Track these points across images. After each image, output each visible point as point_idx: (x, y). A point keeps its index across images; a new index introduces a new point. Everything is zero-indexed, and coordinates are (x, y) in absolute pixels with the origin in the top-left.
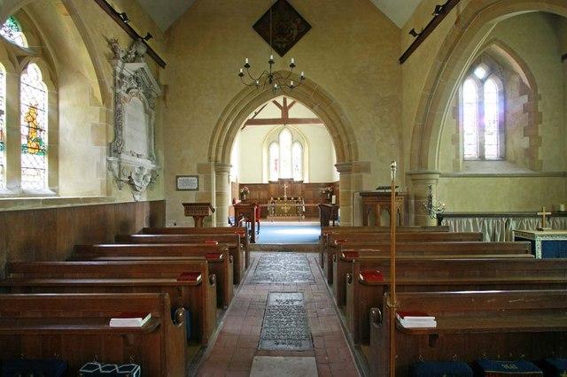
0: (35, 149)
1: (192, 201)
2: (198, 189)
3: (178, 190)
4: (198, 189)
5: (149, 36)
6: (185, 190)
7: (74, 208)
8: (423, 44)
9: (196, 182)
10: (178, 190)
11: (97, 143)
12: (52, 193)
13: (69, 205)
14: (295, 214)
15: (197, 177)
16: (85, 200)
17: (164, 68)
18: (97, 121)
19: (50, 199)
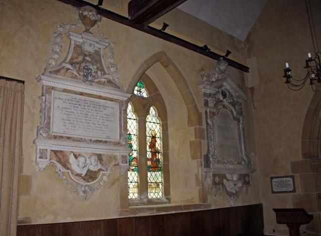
0: (118, 144)
1: (290, 206)
2: (294, 191)
3: (273, 192)
4: (294, 191)
5: (228, 53)
6: (281, 192)
7: (178, 213)
8: (127, 8)
9: (291, 183)
10: (273, 192)
11: (194, 158)
12: (166, 200)
13: (173, 212)
14: (126, 111)
15: (292, 177)
16: (186, 207)
17: (248, 72)
18: (193, 139)
19: (168, 207)
